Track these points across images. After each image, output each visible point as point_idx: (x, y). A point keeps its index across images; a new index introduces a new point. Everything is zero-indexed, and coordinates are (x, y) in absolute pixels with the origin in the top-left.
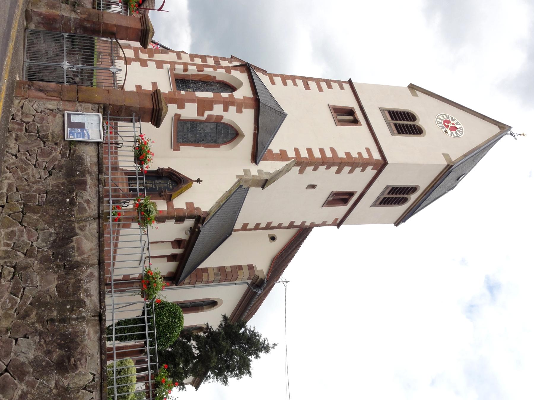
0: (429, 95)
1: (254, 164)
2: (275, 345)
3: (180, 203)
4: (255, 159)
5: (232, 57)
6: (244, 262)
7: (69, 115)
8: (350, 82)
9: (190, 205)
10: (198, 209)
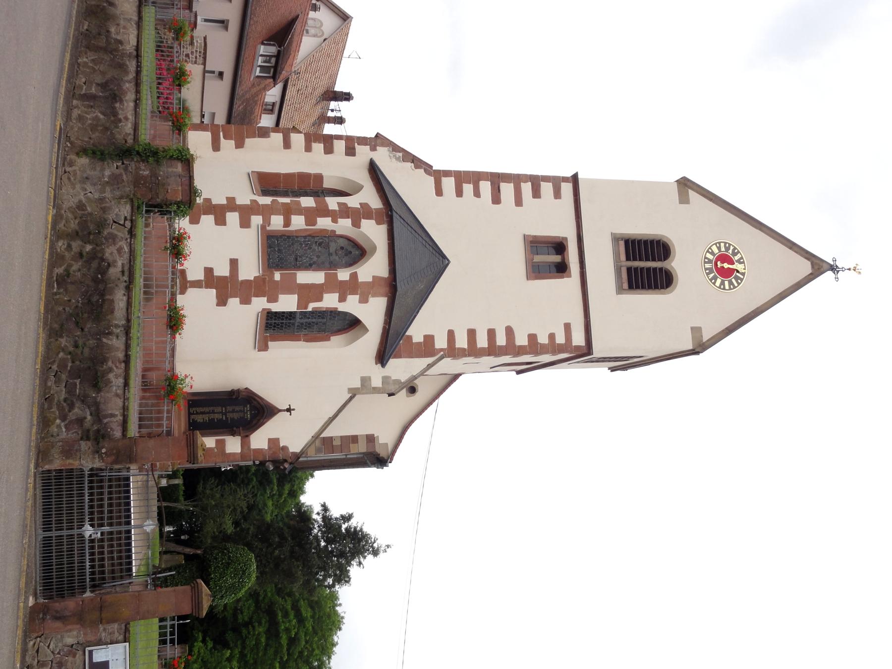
0: (711, 200)
1: (379, 365)
2: (388, 546)
3: (259, 440)
4: (382, 358)
5: (378, 136)
6: (360, 430)
7: (91, 652)
8: (575, 179)
9: (274, 442)
10: (285, 448)
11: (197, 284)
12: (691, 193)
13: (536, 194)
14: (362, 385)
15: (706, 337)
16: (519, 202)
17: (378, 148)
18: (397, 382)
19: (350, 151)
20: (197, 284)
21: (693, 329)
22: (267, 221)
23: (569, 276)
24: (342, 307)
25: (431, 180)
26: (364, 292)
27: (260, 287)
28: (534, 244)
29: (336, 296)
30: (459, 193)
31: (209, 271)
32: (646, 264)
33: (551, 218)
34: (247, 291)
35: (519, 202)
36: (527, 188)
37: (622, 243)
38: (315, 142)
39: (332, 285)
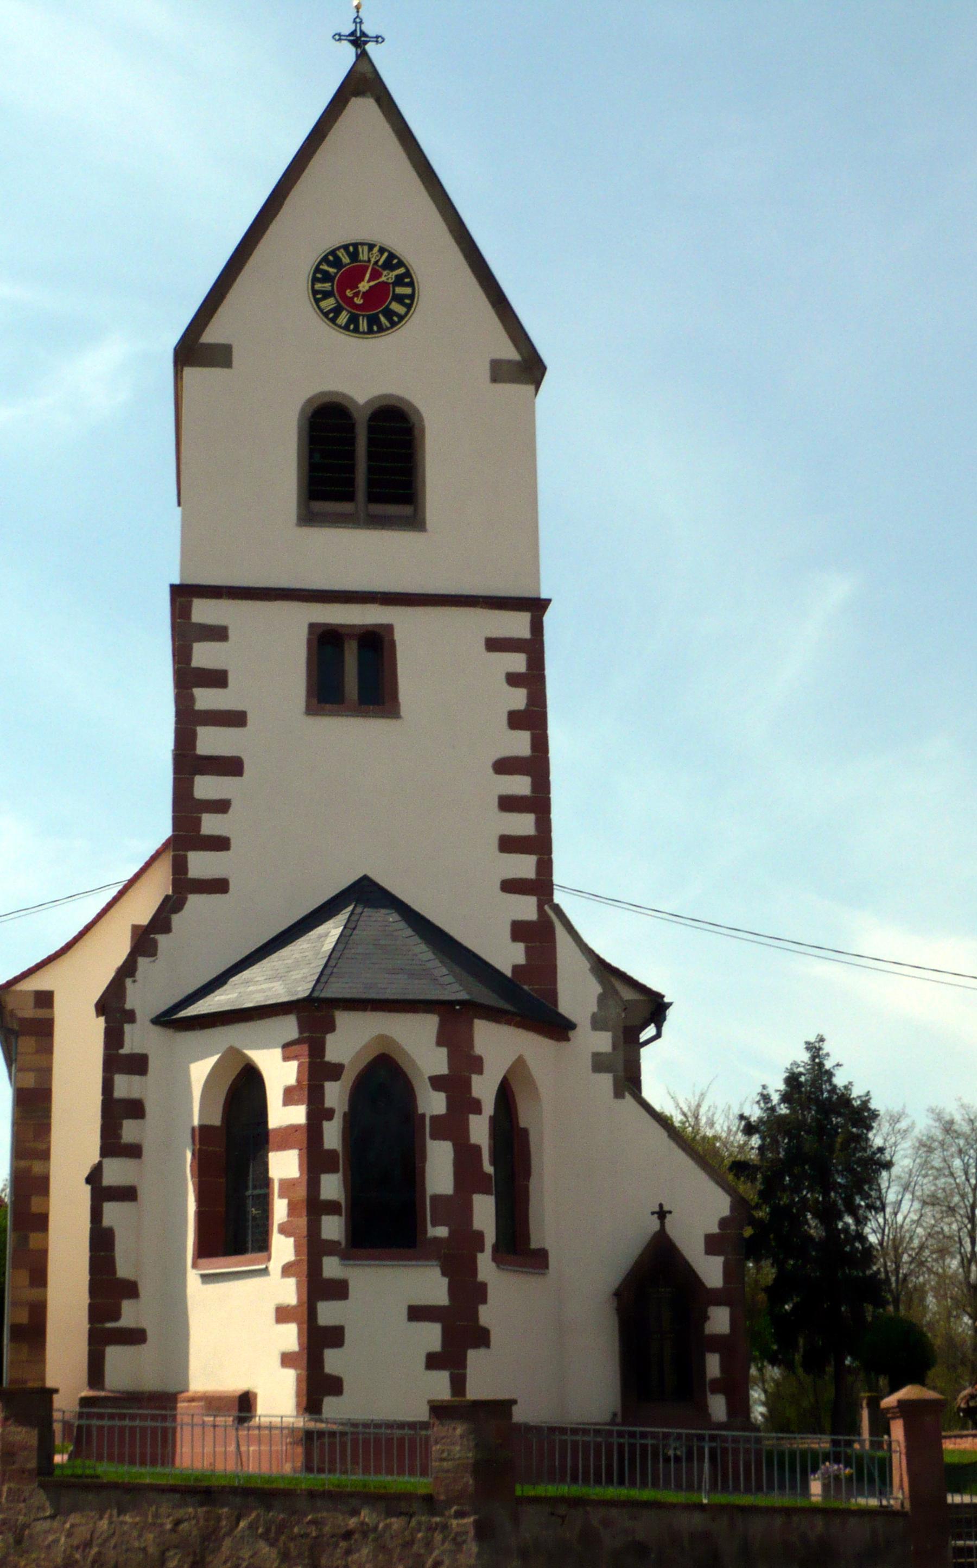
1: (571, 1034)
3: (711, 1271)
4: (559, 1028)
9: (713, 1245)
11: (458, 1384)
12: (210, 336)
13: (218, 679)
14: (607, 1070)
15: (510, 353)
16: (236, 719)
17: (128, 1006)
18: (602, 999)
19: (138, 1065)
20: (458, 1384)
21: (496, 377)
22: (331, 1248)
23: (389, 628)
24: (489, 1108)
25: (194, 901)
26: (465, 1063)
27: (458, 1261)
28: (325, 693)
29: (473, 1118)
30: (220, 844)
31: (433, 1362)
32: (362, 462)
33: (267, 656)
34: (467, 1293)
35: (236, 719)
36: (206, 698)
37: (318, 506)
38: (120, 1137)
39: (452, 1127)
